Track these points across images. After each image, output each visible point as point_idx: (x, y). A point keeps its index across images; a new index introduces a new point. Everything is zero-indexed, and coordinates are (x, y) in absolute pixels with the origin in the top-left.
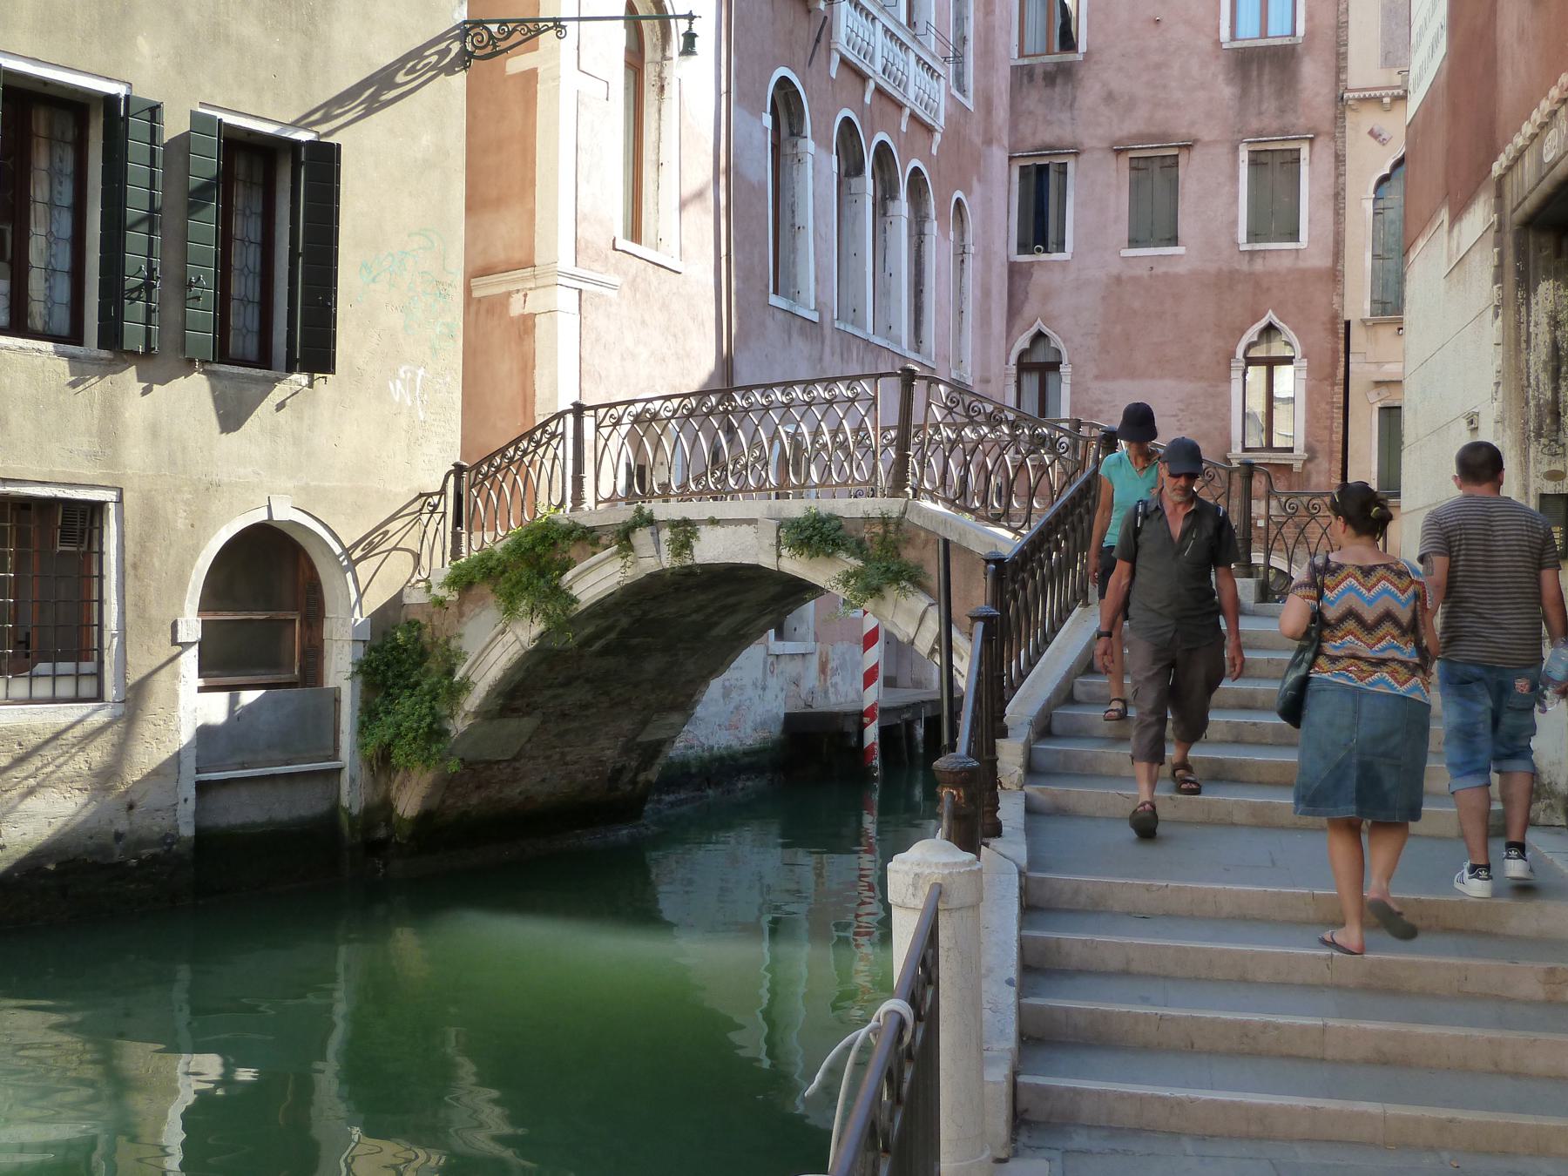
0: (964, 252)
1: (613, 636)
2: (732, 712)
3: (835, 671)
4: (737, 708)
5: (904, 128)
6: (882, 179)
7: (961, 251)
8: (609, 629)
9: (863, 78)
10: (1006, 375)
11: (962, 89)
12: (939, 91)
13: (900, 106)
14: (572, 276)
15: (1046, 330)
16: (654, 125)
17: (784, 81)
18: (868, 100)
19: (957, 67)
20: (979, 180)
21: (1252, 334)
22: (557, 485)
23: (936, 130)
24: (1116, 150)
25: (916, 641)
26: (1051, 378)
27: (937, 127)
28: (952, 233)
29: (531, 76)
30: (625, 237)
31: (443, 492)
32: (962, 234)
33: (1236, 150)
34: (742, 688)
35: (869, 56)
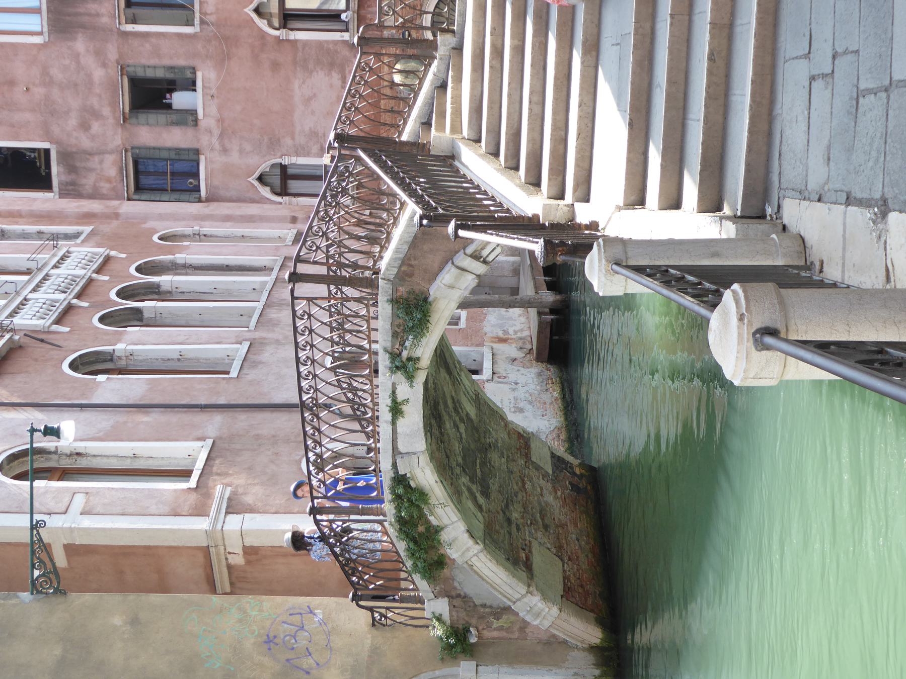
0: (199, 234)
1: (474, 488)
2: (533, 406)
3: (506, 332)
4: (530, 403)
5: (107, 278)
6: (144, 294)
7: (197, 237)
8: (469, 490)
9: (69, 308)
10: (290, 204)
11: (77, 235)
12: (79, 252)
13: (90, 281)
14: (216, 519)
15: (257, 175)
16: (105, 460)
17: (72, 366)
18: (85, 304)
19: (61, 238)
20: (145, 223)
21: (262, 24)
22: (367, 526)
23: (108, 254)
24: (124, 121)
25: (478, 273)
26: (290, 171)
27: (106, 254)
28: (185, 243)
29: (71, 550)
30: (188, 481)
31: (371, 609)
32: (184, 237)
33: (126, 34)
34: (516, 399)
35: (53, 303)
